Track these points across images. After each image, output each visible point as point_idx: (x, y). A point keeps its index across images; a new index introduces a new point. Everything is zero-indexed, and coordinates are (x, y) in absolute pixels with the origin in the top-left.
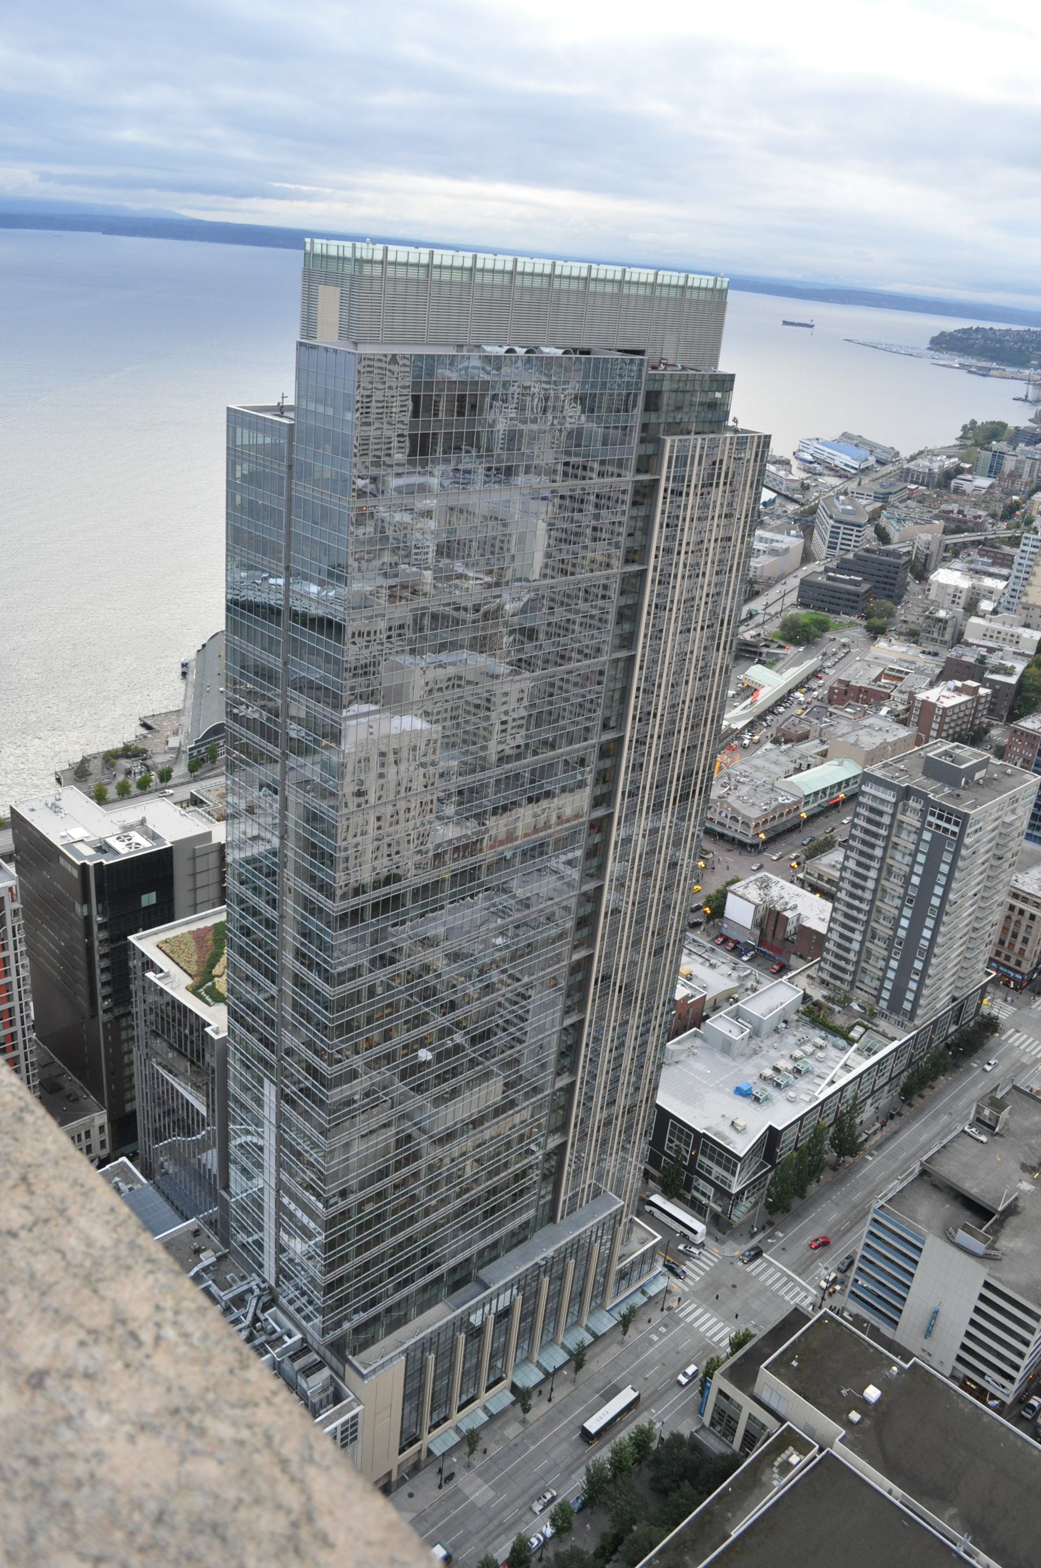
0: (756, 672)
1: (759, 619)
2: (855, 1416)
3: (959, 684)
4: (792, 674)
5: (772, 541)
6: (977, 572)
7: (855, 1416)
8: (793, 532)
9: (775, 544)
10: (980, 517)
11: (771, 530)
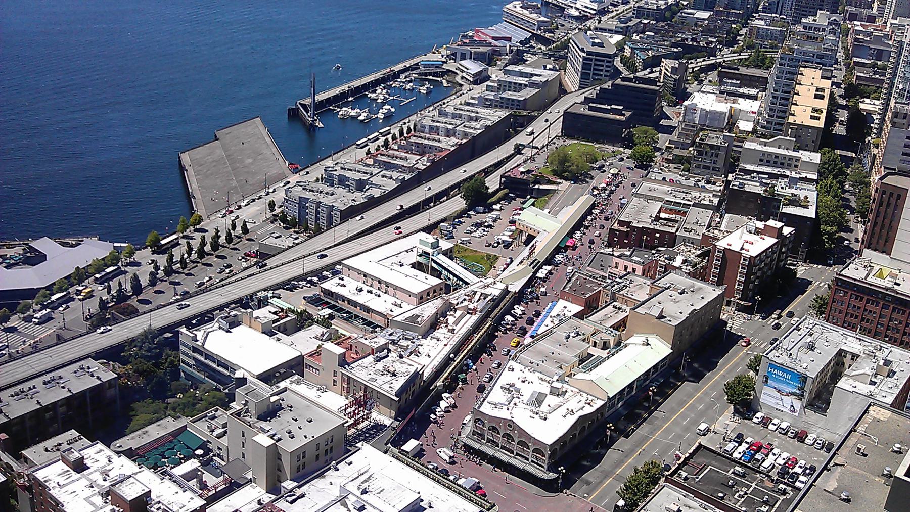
0: (531, 216)
1: (528, 152)
2: (657, 235)
3: (760, 225)
4: (569, 214)
5: (532, 75)
6: (729, 94)
7: (657, 235)
8: (549, 66)
9: (534, 78)
10: (711, 42)
11: (529, 65)
